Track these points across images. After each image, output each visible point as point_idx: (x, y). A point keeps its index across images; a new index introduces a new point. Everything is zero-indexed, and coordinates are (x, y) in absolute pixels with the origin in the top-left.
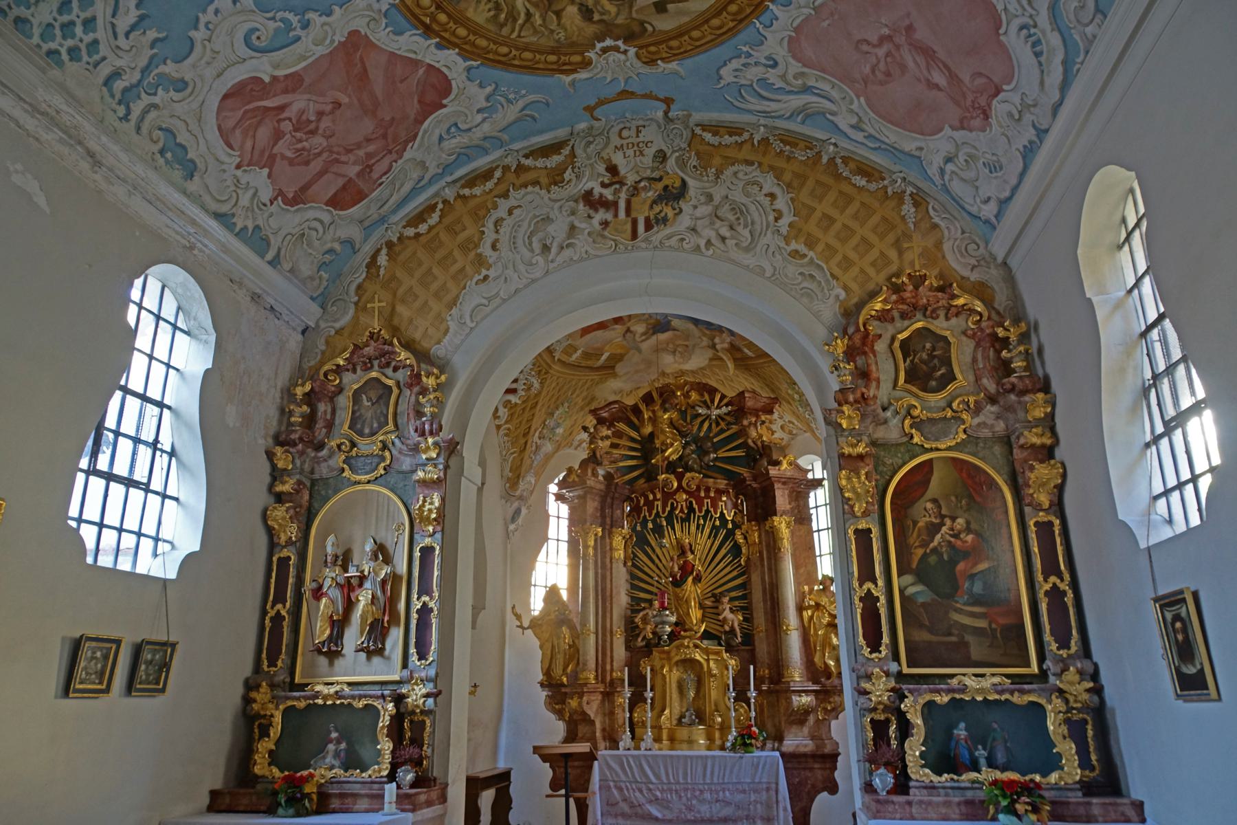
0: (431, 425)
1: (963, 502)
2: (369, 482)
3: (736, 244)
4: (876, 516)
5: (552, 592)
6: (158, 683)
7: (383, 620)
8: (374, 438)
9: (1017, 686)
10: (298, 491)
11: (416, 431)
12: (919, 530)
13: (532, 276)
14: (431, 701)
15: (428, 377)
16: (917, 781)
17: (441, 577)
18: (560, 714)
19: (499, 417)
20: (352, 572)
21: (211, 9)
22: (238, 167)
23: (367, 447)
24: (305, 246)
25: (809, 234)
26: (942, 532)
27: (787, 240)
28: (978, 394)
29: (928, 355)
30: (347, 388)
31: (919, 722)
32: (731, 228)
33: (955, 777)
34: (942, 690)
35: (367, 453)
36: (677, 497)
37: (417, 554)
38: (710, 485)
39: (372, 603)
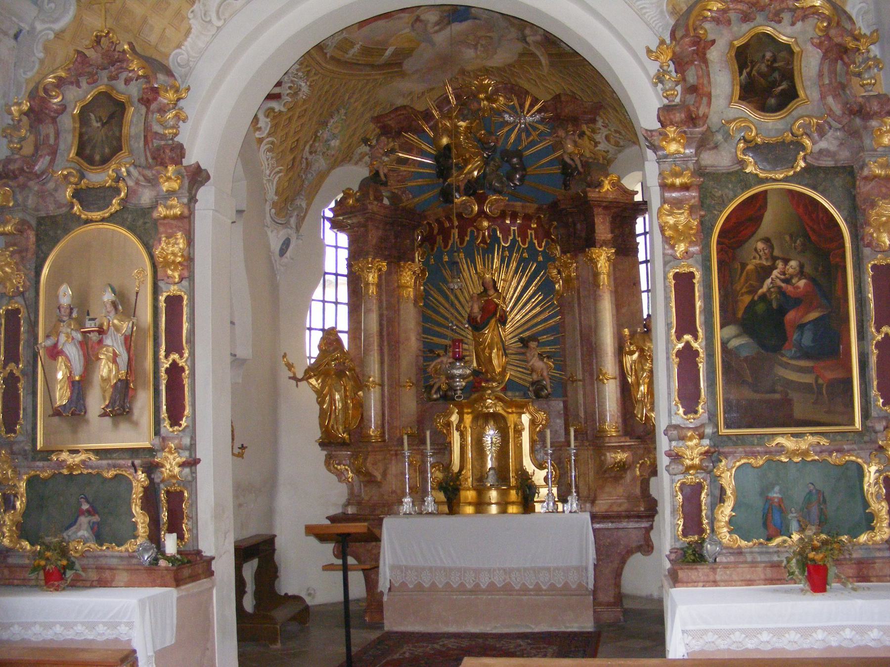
2: (103, 220)
5: (330, 337)
12: (747, 273)
14: (187, 470)
19: (259, 129)
26: (773, 276)
29: (768, 66)
34: (759, 452)
37: (162, 305)
38: (518, 209)
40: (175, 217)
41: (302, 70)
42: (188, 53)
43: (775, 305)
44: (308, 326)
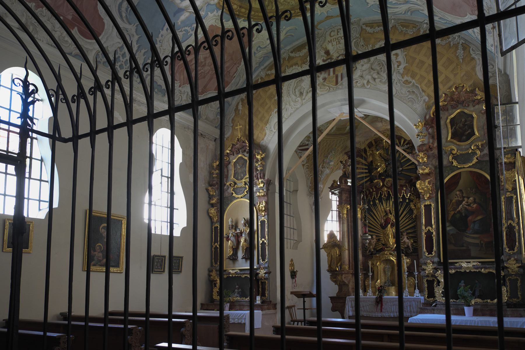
1: (474, 190)
3: (380, 81)
4: (434, 199)
6: (179, 270)
9: (484, 266)
13: (296, 107)
14: (267, 275)
16: (440, 302)
17: (268, 231)
18: (336, 282)
20: (238, 231)
21: (160, 35)
22: (180, 86)
24: (210, 108)
25: (413, 71)
26: (463, 204)
27: (403, 75)
28: (483, 141)
29: (463, 124)
31: (442, 280)
32: (378, 73)
33: (455, 300)
36: (383, 189)
37: (259, 223)
42: (266, 141)
43: (463, 214)
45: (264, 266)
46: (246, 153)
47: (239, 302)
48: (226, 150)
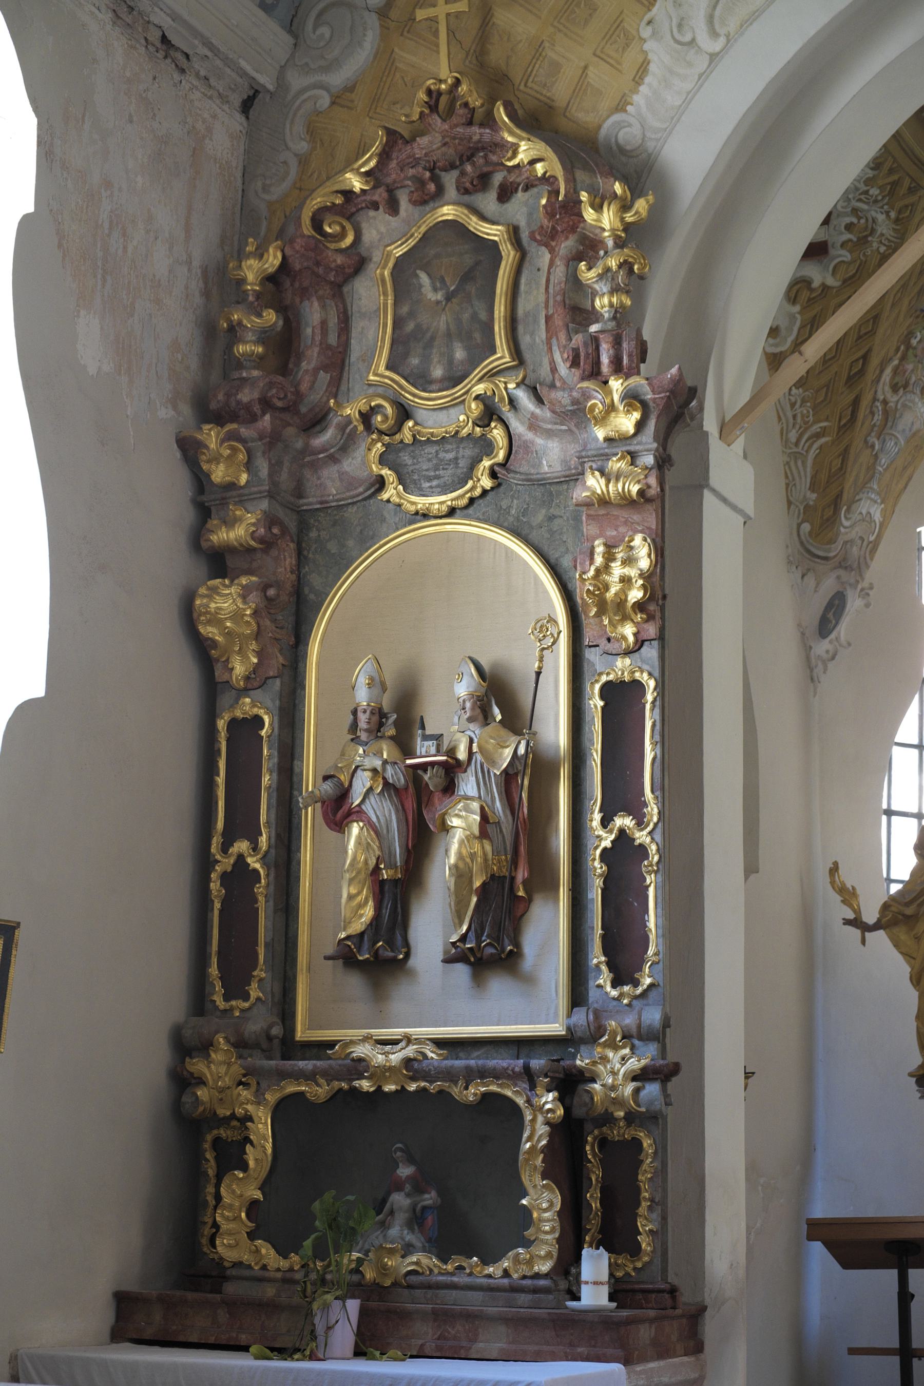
0: (617, 342)
2: (452, 512)
7: (513, 879)
8: (459, 390)
10: (267, 544)
11: (575, 363)
14: (652, 1089)
15: (598, 208)
17: (663, 763)
23: (442, 416)
30: (377, 256)
35: (440, 431)
37: (595, 703)
39: (484, 834)
40: (628, 502)
41: (880, 183)
44: (885, 806)
45: (629, 1020)
46: (492, 195)
47: (429, 1286)
48: (343, 171)
